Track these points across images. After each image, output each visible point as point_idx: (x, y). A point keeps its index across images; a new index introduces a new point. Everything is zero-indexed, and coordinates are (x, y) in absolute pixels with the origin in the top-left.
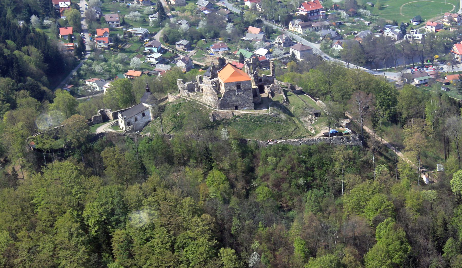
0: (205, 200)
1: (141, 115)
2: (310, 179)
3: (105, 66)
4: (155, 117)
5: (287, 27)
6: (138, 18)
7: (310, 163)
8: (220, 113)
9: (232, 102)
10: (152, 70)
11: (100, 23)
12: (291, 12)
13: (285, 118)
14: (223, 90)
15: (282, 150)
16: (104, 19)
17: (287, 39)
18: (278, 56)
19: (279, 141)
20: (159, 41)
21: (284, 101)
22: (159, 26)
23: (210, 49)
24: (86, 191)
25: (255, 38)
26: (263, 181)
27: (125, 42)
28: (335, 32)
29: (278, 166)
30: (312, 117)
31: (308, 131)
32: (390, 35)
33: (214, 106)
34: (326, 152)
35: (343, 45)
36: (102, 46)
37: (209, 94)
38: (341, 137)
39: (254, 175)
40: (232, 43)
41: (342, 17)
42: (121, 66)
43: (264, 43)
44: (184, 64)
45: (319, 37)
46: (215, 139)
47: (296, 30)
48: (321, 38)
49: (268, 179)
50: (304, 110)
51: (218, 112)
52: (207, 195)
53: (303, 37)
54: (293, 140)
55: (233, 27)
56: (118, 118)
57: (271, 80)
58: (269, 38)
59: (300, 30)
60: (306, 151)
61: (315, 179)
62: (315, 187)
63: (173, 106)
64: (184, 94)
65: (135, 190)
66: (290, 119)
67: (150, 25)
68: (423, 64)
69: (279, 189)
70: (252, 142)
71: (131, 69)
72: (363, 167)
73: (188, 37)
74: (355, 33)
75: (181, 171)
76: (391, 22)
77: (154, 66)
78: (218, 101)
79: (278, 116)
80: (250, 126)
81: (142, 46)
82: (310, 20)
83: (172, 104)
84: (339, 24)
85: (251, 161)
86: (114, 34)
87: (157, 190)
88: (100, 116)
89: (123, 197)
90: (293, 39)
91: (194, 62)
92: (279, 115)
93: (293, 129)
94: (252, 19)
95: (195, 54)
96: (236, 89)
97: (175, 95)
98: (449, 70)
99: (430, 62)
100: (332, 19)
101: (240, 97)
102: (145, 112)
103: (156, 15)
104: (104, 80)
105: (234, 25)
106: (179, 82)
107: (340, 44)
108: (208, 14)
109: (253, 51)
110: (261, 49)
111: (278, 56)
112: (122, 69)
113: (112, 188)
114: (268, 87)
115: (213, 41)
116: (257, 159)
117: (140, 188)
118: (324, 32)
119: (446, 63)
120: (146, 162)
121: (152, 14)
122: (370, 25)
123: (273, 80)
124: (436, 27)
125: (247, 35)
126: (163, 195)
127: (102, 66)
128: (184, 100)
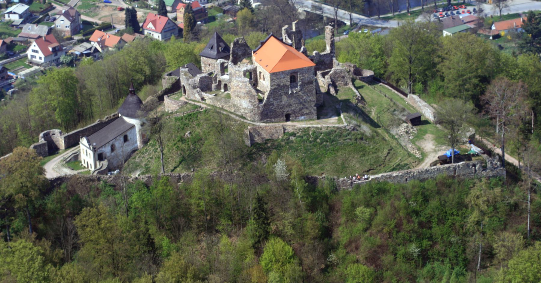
1: (122, 139)
2: (426, 243)
4: (145, 142)
10: (15, 36)
13: (370, 131)
14: (265, 84)
15: (378, 194)
19: (371, 177)
26: (347, 253)
29: (374, 223)
30: (407, 127)
31: (410, 155)
33: (251, 116)
34: (450, 191)
37: (242, 95)
38: (471, 163)
44: (68, 23)
46: (262, 179)
49: (357, 248)
57: (327, 60)
60: (418, 192)
61: (435, 243)
62: (436, 257)
63: (176, 119)
66: (378, 134)
69: (378, 267)
70: (326, 182)
75: (202, 241)
78: (258, 107)
79: (358, 128)
80: (315, 150)
83: (175, 116)
85: (327, 216)
88: (43, 145)
91: (83, 17)
92: (359, 126)
93: (386, 151)
96: (288, 84)
98: (495, 12)
101: (295, 97)
102: (128, 133)
106: (185, 75)
114: (323, 75)
116: (337, 212)
128: (196, 107)
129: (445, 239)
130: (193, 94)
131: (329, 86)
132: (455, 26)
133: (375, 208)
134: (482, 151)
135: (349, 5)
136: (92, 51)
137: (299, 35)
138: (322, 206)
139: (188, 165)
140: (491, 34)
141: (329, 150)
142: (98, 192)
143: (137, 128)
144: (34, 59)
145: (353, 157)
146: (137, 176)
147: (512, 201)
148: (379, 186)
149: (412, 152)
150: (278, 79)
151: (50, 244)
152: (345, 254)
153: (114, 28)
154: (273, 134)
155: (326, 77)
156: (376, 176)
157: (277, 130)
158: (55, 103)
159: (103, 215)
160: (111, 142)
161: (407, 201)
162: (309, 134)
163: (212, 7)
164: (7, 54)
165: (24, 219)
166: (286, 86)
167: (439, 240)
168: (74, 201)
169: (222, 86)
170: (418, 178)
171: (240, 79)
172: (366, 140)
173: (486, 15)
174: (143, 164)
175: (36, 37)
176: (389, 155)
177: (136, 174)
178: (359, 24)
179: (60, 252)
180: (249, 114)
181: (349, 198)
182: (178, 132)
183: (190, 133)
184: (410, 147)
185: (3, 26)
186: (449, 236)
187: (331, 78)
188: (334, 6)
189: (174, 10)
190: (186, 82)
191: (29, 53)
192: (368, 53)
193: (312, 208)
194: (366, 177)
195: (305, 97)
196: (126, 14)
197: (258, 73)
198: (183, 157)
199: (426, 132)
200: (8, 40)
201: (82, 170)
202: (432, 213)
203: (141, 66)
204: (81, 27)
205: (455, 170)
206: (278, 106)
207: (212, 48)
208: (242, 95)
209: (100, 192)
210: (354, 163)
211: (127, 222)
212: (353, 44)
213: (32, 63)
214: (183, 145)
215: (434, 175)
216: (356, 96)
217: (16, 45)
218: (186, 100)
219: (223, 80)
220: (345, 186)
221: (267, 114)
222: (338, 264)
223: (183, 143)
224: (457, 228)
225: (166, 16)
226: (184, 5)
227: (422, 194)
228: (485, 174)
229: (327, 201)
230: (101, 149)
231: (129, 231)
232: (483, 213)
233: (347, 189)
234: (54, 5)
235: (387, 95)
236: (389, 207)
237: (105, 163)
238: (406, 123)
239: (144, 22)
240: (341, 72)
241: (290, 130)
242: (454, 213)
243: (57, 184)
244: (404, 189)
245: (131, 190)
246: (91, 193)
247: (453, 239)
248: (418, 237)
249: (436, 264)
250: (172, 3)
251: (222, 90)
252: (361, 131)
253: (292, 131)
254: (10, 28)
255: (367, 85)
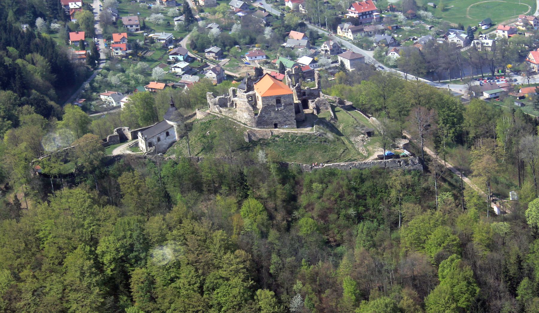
0: (239, 234)
1: (165, 134)
2: (361, 209)
3: (123, 77)
4: (181, 137)
5: (335, 32)
6: (161, 21)
7: (362, 190)
8: (257, 132)
9: (271, 120)
10: (177, 82)
11: (117, 27)
12: (340, 14)
13: (333, 138)
14: (260, 105)
15: (329, 175)
16: (121, 22)
17: (335, 45)
18: (324, 66)
19: (326, 165)
20: (186, 48)
21: (331, 118)
22: (186, 31)
23: (245, 57)
24: (101, 223)
25: (297, 44)
26: (307, 212)
27: (146, 49)
28: (391, 37)
29: (324, 194)
30: (364, 137)
31: (359, 154)
32: (455, 41)
33: (250, 124)
34: (381, 177)
35: (400, 52)
36: (119, 54)
37: (244, 110)
38: (397, 160)
39: (297, 204)
40: (271, 51)
41: (399, 20)
42: (141, 78)
43: (308, 50)
44: (214, 75)
45: (372, 43)
46: (251, 162)
47: (345, 35)
48: (375, 45)
49: (313, 209)
50: (355, 128)
51: (255, 131)
52: (241, 228)
53: (354, 43)
54: (342, 164)
55: (272, 32)
56: (137, 138)
57: (316, 93)
58: (314, 44)
59: (350, 35)
61: (368, 209)
62: (368, 218)
63: (201, 124)
64: (215, 110)
65: (157, 222)
66: (338, 140)
67: (175, 29)
68: (493, 75)
69: (326, 221)
70: (294, 166)
71: (153, 81)
72: (423, 195)
73: (219, 43)
74: (414, 39)
75: (211, 199)
76: (456, 25)
77: (180, 77)
78: (254, 118)
79: (324, 135)
80: (292, 147)
81: (166, 53)
82: (361, 23)
83: (201, 121)
84: (395, 28)
85: (293, 188)
86: (133, 40)
87: (183, 221)
88: (116, 136)
89: (144, 230)
90: (342, 46)
91: (227, 72)
92: (326, 134)
93: (342, 150)
94: (294, 23)
95: (228, 64)
96: (275, 104)
97: (204, 111)
98: (524, 82)
99: (502, 72)
100: (388, 22)
101: (280, 113)
102: (169, 131)
103: (182, 18)
104: (121, 94)
105: (273, 29)
106: (209, 96)
107: (397, 51)
108: (243, 16)
109: (295, 59)
110: (304, 57)
111: (324, 66)
112: (143, 81)
113: (130, 220)
114: (312, 102)
115: (249, 47)
116: (300, 186)
117: (164, 219)
118: (378, 37)
119: (520, 74)
120: (170, 189)
121: (177, 17)
122: (432, 29)
123: (319, 93)
124: (508, 31)
125: (289, 40)
126: (190, 227)
127: (119, 77)
128: (215, 116)
247: (380, 208)
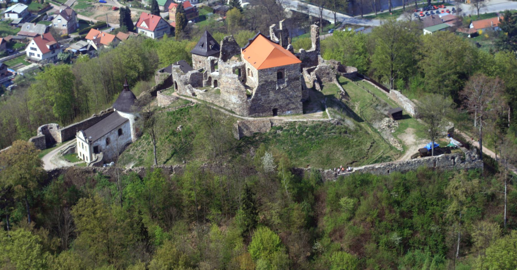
1: (117, 133)
4: (139, 135)
10: (15, 34)
13: (354, 125)
14: (253, 80)
15: (361, 185)
19: (355, 169)
26: (332, 241)
29: (357, 213)
30: (389, 121)
31: (391, 148)
33: (240, 111)
34: (430, 182)
37: (232, 91)
38: (450, 155)
44: (65, 22)
46: (250, 170)
49: (341, 237)
57: (312, 58)
60: (400, 183)
61: (416, 232)
62: (416, 245)
63: (169, 114)
66: (361, 128)
69: (361, 254)
70: (312, 173)
75: (193, 230)
78: (247, 102)
79: (342, 123)
80: (301, 143)
83: (167, 110)
85: (313, 206)
88: (41, 138)
91: (80, 17)
92: (344, 121)
93: (369, 144)
96: (275, 80)
98: (473, 11)
101: (282, 93)
102: (122, 127)
106: (177, 71)
114: (309, 72)
116: (322, 202)
128: (188, 102)
129: (425, 228)
130: (185, 90)
131: (314, 82)
132: (435, 25)
133: (359, 198)
134: (461, 144)
135: (334, 5)
136: (88, 49)
137: (286, 34)
138: (308, 197)
139: (180, 158)
140: (469, 33)
141: (314, 143)
142: (94, 184)
143: (131, 122)
144: (32, 56)
145: (338, 150)
146: (131, 168)
147: (489, 192)
148: (362, 177)
149: (394, 145)
150: (266, 75)
151: (48, 232)
152: (329, 242)
153: (109, 27)
154: (261, 128)
155: (312, 73)
156: (360, 168)
157: (264, 124)
158: (52, 98)
159: (98, 205)
160: (106, 135)
161: (389, 192)
162: (295, 128)
163: (203, 6)
164: (7, 51)
165: (23, 209)
166: (273, 82)
167: (420, 229)
168: (70, 191)
169: (212, 82)
170: (400, 170)
171: (229, 76)
172: (350, 134)
173: (464, 14)
174: (137, 157)
175: (34, 35)
176: (372, 148)
177: (130, 166)
178: (344, 23)
179: (57, 241)
180: (238, 109)
181: (334, 189)
182: (170, 126)
183: (182, 127)
184: (391, 140)
185: (3, 25)
186: (429, 225)
187: (316, 75)
188: (319, 6)
189: (166, 10)
190: (177, 78)
191: (28, 50)
192: (352, 51)
193: (299, 198)
194: (349, 168)
195: (291, 93)
196: (120, 13)
197: (247, 69)
198: (175, 150)
199: (407, 126)
200: (8, 38)
201: (79, 163)
202: (413, 203)
203: (134, 63)
204: (78, 25)
205: (435, 163)
206: (266, 101)
207: (202, 46)
208: (232, 91)
209: (96, 183)
210: (338, 155)
211: (121, 212)
212: (338, 42)
213: (30, 61)
214: (175, 139)
215: (414, 167)
216: (341, 91)
217: (16, 43)
218: (178, 96)
219: (214, 77)
220: (330, 177)
221: (255, 109)
222: (323, 252)
223: (175, 137)
224: (437, 217)
225: (159, 15)
226: (176, 4)
227: (403, 186)
228: (463, 166)
229: (312, 192)
230: (96, 142)
231: (123, 221)
232: (462, 204)
233: (332, 180)
234: (52, 5)
235: (370, 91)
236: (372, 197)
237: (100, 155)
238: (388, 117)
239: (138, 21)
240: (326, 68)
241: (277, 124)
242: (434, 204)
243: (55, 176)
244: (386, 181)
245: (125, 181)
246: (87, 184)
247: (432, 228)
248: (399, 226)
249: (417, 252)
250: (164, 3)
251: (213, 86)
252: (345, 125)
253: (279, 125)
254: (10, 26)
255: (351, 81)
